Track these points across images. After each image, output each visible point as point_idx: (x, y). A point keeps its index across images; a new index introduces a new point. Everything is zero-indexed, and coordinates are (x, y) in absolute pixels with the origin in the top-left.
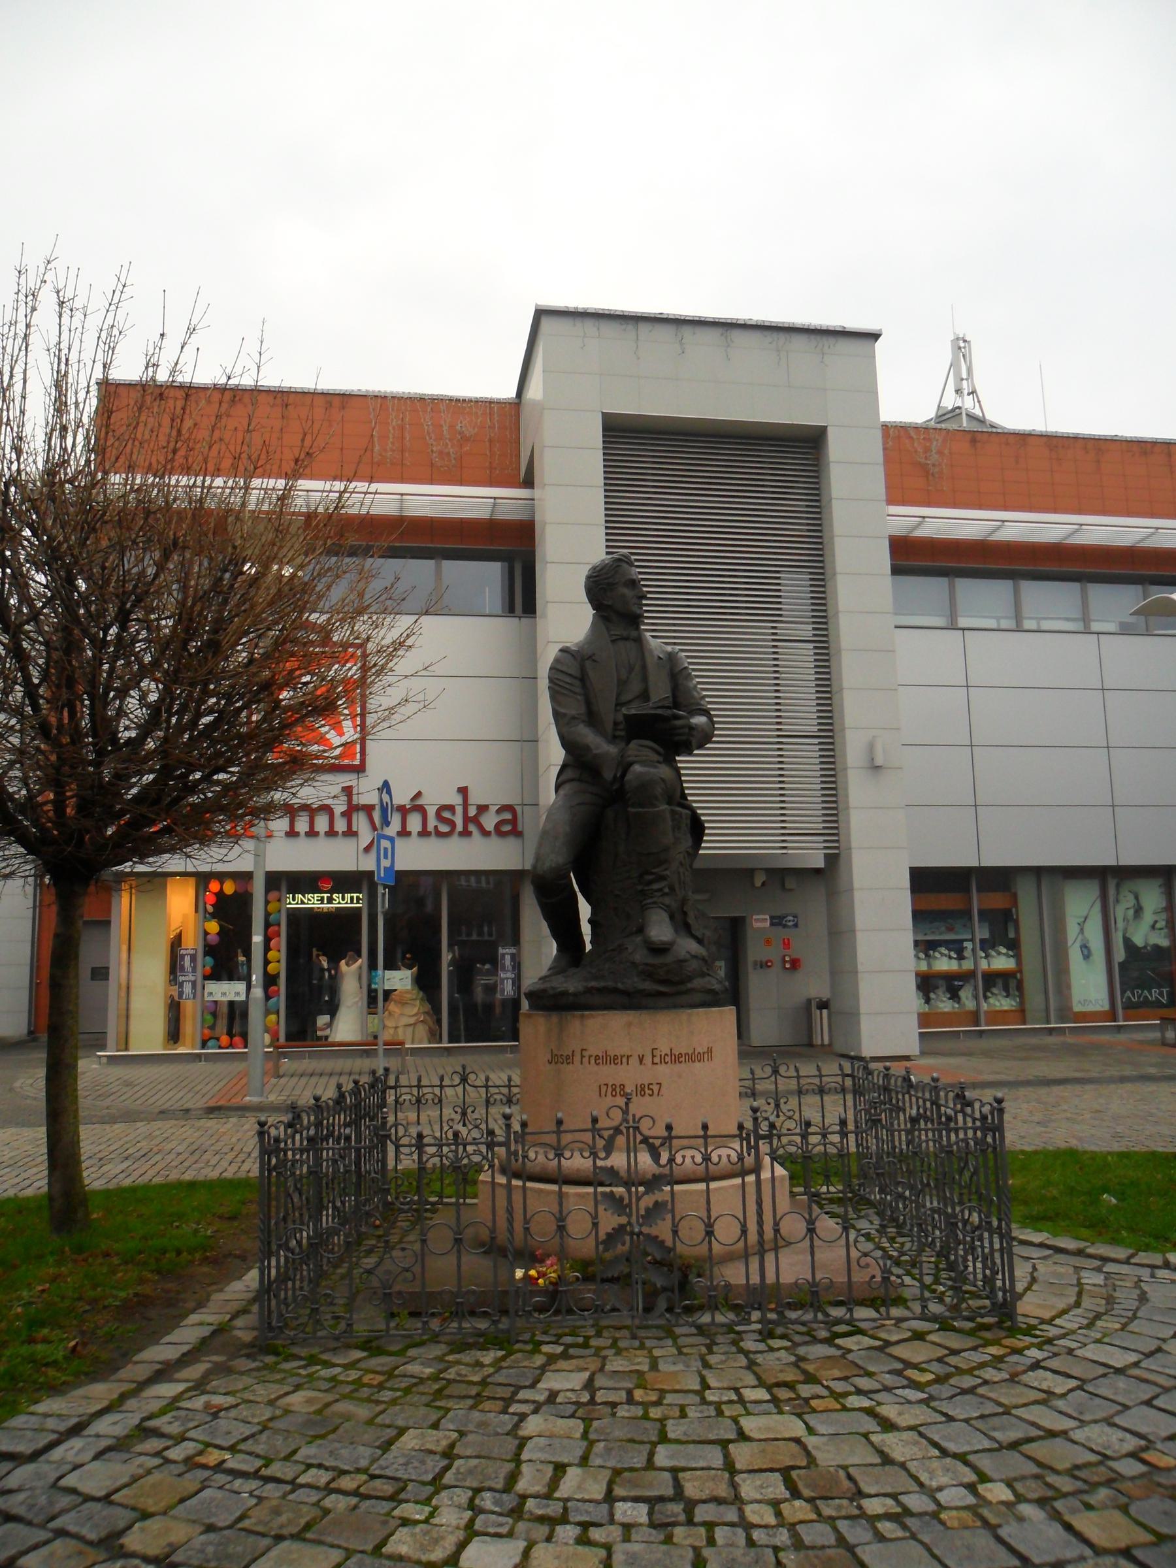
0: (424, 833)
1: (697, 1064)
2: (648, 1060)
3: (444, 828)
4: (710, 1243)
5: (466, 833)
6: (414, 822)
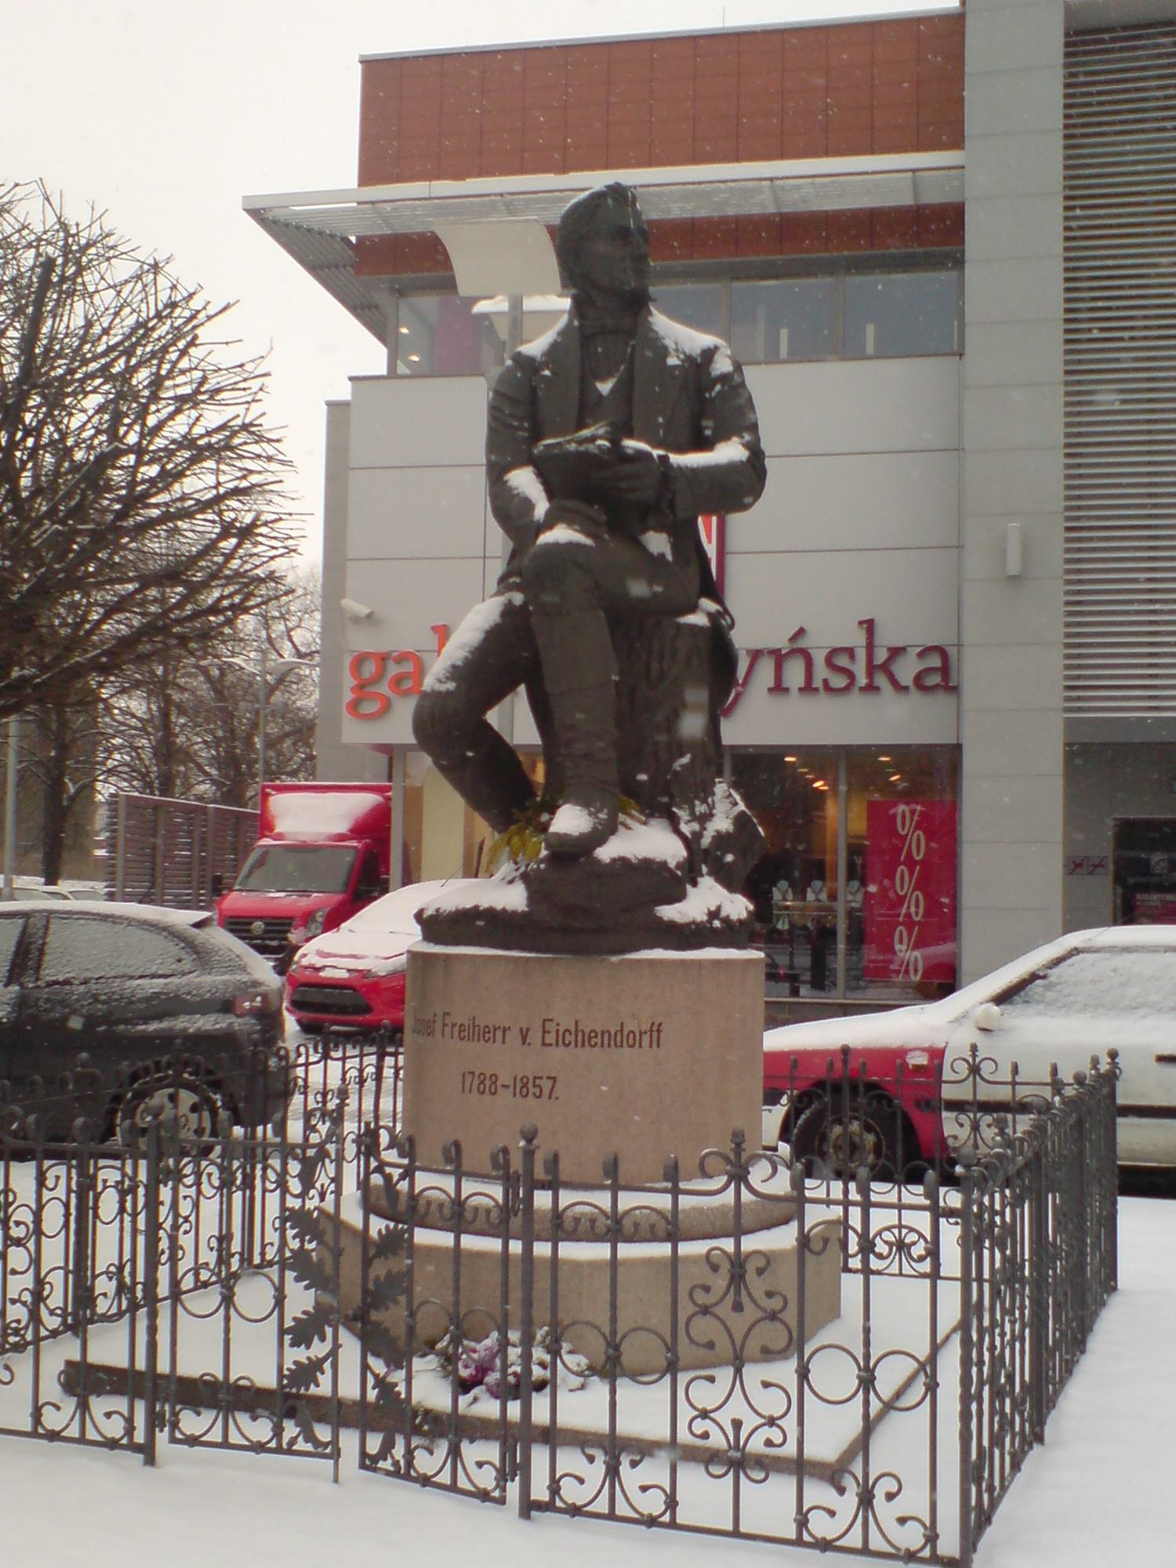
0: (808, 688)
1: (626, 1050)
2: (535, 1037)
3: (839, 681)
4: (227, 1319)
5: (871, 688)
6: (795, 673)
